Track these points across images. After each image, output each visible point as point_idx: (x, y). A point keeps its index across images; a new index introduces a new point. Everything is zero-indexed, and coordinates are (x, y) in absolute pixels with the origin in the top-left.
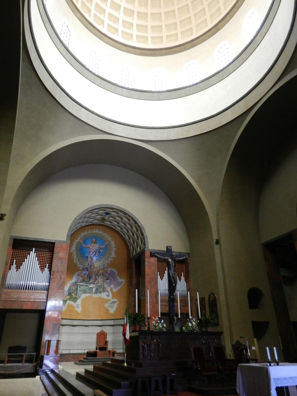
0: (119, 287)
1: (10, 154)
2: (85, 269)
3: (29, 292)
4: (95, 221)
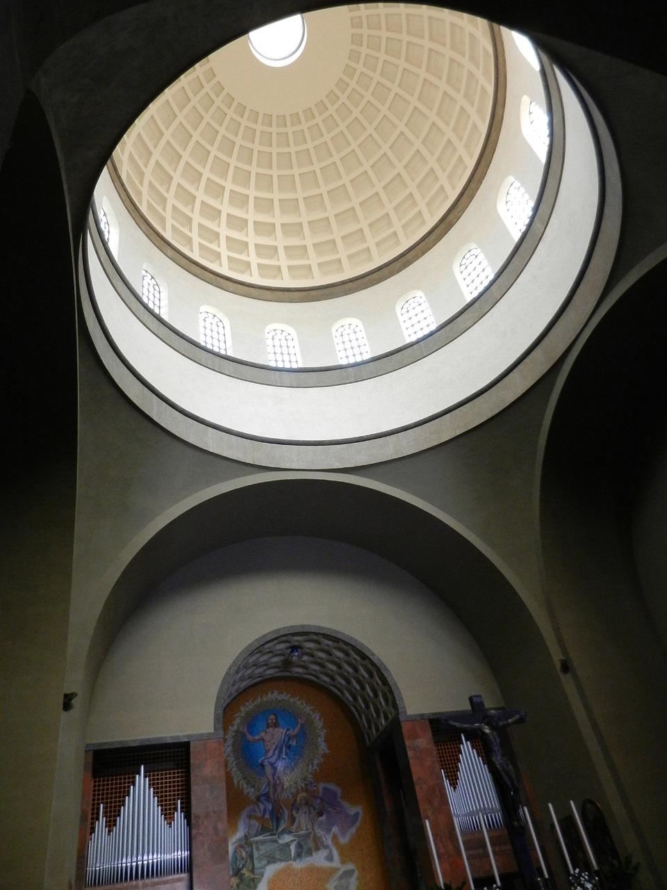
0: (353, 830)
1: (71, 552)
2: (262, 798)
3: (145, 886)
4: (269, 672)
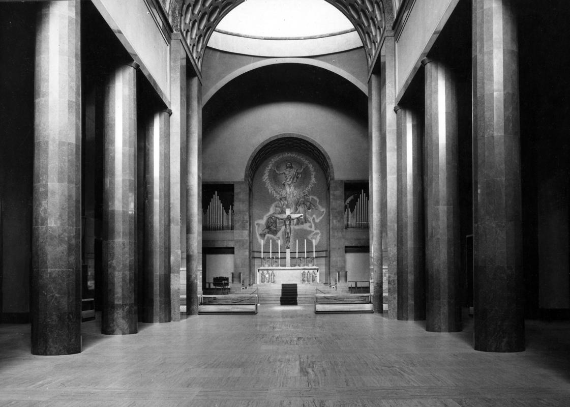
0: (321, 218)
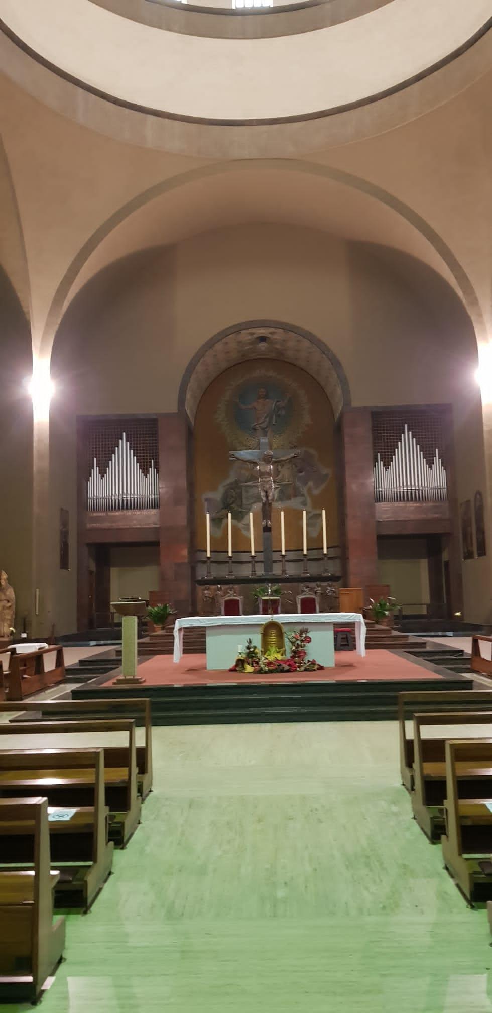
0: (323, 486)
